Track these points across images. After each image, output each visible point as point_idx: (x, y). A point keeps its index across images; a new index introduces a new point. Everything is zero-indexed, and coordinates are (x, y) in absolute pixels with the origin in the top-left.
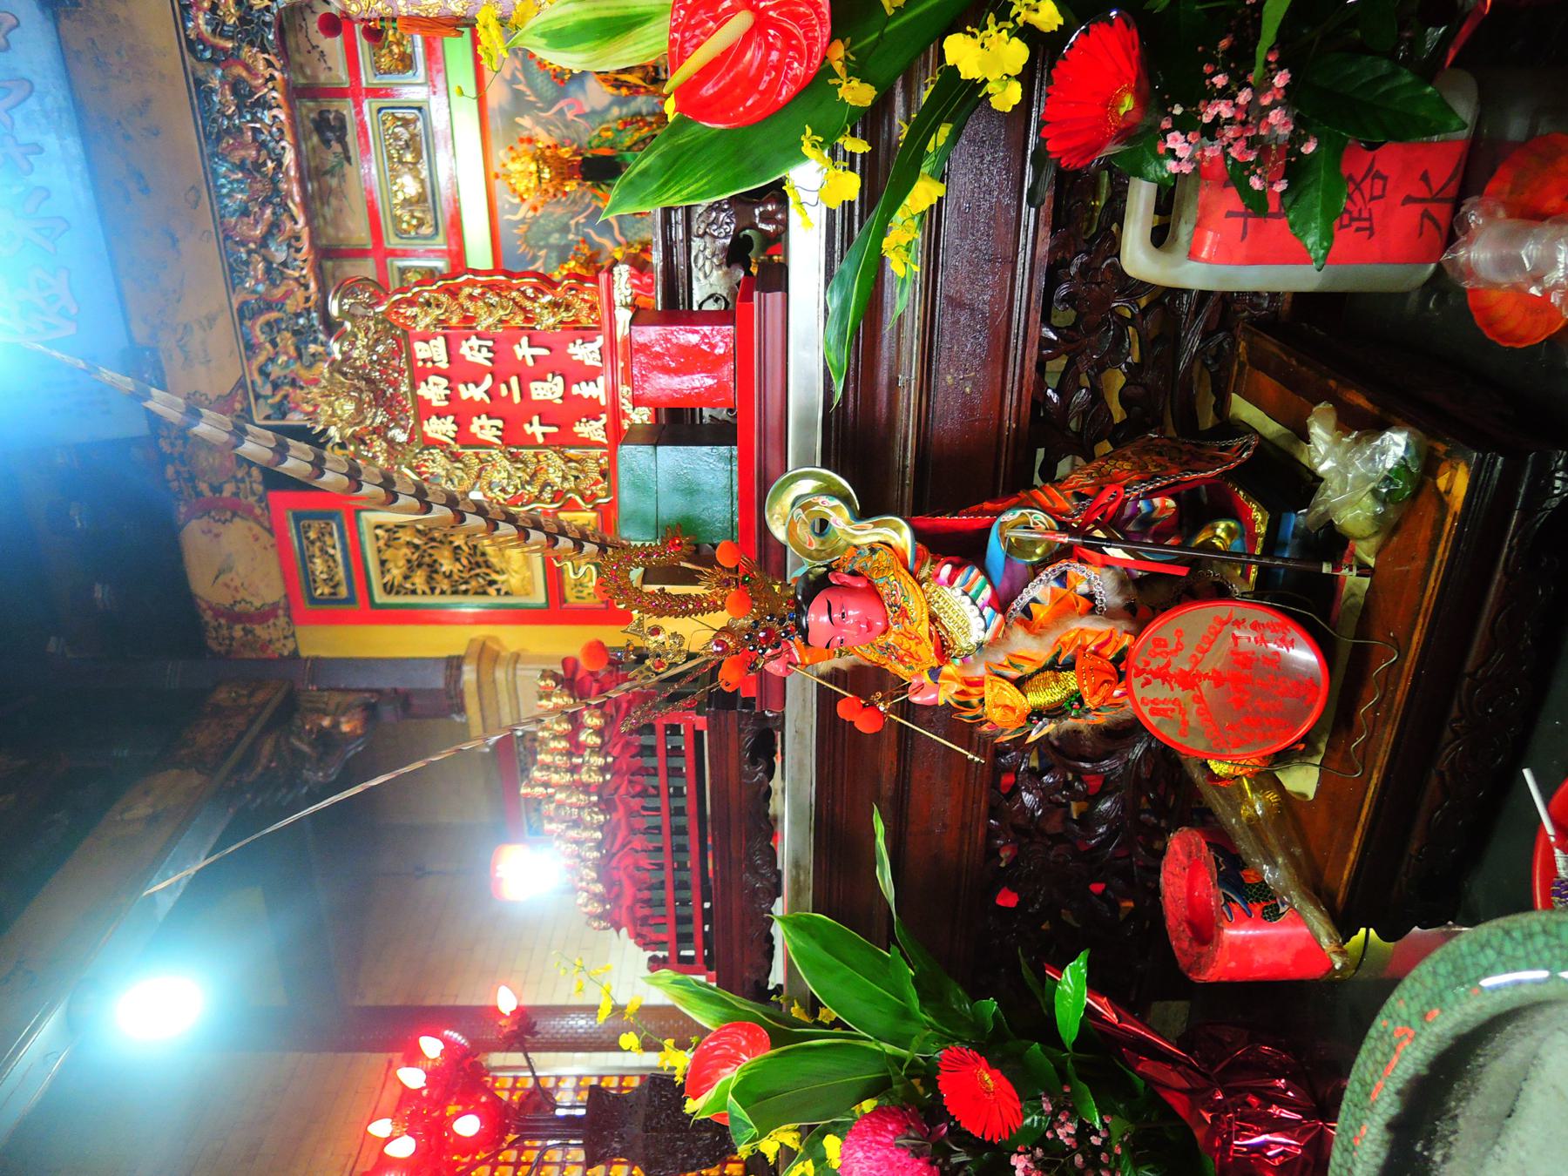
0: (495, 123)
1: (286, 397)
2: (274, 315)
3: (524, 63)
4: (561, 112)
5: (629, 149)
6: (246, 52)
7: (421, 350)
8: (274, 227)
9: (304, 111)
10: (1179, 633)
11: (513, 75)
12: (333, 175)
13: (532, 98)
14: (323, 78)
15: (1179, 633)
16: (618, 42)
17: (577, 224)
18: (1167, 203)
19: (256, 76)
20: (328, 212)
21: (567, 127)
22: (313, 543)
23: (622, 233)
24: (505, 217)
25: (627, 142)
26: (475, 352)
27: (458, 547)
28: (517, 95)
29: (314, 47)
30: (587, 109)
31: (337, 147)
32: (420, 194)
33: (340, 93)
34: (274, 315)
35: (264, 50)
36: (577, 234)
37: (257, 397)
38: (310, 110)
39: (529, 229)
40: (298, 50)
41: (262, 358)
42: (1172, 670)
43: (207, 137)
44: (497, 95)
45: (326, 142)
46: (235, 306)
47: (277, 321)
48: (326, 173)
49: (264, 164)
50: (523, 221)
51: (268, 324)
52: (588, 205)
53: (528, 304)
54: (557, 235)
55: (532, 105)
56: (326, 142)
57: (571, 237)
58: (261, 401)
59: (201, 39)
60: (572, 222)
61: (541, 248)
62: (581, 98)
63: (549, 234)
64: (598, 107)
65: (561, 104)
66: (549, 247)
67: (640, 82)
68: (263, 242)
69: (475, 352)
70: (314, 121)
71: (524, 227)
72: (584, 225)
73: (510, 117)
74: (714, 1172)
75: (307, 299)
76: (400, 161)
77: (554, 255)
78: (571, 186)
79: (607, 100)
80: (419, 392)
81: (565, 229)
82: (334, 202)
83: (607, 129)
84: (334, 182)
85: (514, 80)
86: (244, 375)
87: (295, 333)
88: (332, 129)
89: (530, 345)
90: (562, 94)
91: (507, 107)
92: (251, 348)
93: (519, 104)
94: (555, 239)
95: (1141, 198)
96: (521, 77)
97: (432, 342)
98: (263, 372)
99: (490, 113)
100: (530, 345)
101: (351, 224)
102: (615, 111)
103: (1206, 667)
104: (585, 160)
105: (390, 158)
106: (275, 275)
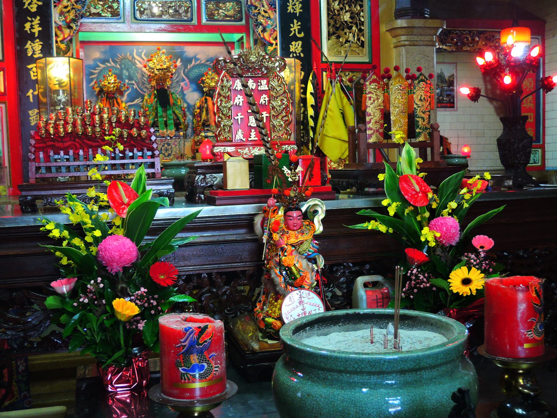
4: (183, 80)
5: (174, 112)
7: (264, 82)
10: (313, 298)
11: (198, 59)
13: (189, 67)
15: (313, 298)
16: (408, 164)
17: (133, 84)
18: (375, 284)
21: (177, 82)
26: (264, 99)
28: (189, 60)
30: (185, 92)
32: (155, 14)
36: (128, 84)
39: (130, 61)
42: (303, 299)
50: (133, 58)
53: (280, 117)
54: (127, 74)
55: (186, 67)
57: (127, 81)
60: (134, 82)
62: (190, 89)
63: (127, 70)
64: (186, 97)
65: (187, 81)
66: (121, 69)
69: (264, 99)
71: (130, 58)
72: (133, 87)
76: (170, 7)
77: (117, 72)
79: (192, 103)
80: (250, 80)
81: (130, 78)
82: (317, 396)
85: (197, 59)
89: (266, 117)
90: (192, 81)
91: (185, 55)
94: (125, 73)
95: (378, 278)
96: (197, 63)
97: (266, 86)
99: (182, 46)
100: (266, 117)
102: (185, 105)
103: (305, 306)
105: (171, 2)
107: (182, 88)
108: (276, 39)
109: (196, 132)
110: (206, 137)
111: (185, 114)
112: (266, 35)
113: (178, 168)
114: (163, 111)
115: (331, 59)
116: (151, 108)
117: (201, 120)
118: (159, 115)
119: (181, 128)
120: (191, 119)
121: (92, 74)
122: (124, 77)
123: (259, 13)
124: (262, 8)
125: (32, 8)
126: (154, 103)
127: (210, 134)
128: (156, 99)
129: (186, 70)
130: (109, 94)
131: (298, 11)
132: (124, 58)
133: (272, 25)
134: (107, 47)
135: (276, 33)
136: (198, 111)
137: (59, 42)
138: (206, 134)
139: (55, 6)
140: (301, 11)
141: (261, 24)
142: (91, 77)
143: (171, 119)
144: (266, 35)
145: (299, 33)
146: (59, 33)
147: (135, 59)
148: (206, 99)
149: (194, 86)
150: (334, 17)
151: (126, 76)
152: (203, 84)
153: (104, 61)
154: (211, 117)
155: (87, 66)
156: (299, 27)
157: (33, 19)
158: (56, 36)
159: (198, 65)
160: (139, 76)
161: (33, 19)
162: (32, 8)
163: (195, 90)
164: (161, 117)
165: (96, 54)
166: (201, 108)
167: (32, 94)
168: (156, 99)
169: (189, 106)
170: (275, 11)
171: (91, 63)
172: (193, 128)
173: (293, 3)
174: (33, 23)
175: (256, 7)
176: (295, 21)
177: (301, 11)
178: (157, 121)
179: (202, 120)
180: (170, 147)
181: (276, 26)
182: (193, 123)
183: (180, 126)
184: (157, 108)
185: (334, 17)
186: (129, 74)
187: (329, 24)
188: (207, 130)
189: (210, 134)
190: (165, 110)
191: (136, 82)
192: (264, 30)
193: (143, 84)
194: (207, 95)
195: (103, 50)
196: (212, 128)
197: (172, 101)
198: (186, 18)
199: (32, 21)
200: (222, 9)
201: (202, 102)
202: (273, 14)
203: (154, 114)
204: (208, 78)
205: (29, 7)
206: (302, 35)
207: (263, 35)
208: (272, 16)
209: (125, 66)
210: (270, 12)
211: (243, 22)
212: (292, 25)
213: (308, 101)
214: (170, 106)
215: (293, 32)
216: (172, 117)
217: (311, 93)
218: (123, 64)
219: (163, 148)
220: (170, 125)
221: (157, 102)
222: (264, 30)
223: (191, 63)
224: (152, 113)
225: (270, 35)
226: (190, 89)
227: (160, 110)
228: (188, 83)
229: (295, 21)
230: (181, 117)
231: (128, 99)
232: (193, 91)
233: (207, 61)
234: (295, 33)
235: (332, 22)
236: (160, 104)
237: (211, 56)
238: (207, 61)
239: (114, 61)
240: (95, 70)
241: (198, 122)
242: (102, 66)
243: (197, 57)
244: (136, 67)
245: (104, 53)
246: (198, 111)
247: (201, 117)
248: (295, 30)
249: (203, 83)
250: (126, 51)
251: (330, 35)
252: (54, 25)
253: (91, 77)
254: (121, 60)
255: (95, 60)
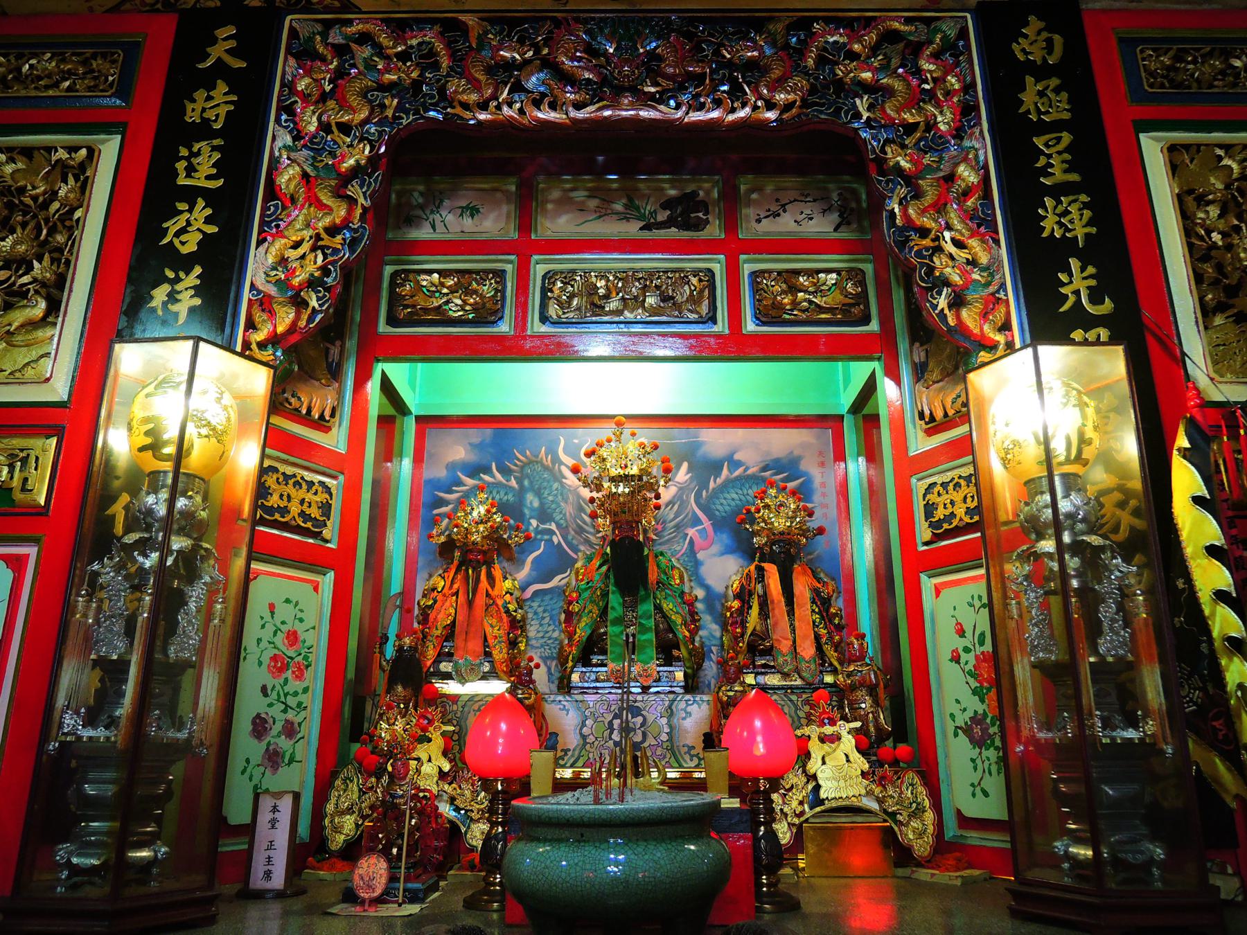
0: (679, 436)
1: (323, 59)
2: (445, 63)
3: (754, 479)
4: (696, 521)
5: (658, 608)
6: (801, 82)
8: (567, 78)
9: (706, 185)
12: (626, 206)
13: (712, 485)
14: (749, 212)
17: (552, 532)
19: (772, 89)
20: (579, 195)
21: (677, 527)
22: (85, 63)
23: (536, 593)
24: (563, 438)
25: (668, 606)
27: (30, 268)
28: (714, 467)
29: (783, 206)
30: (700, 556)
31: (662, 216)
33: (731, 225)
34: (445, 63)
35: (805, 104)
36: (537, 531)
37: (328, 25)
38: (708, 192)
39: (546, 468)
40: (779, 189)
41: (384, 40)
43: (693, 21)
44: (715, 441)
45: (668, 204)
46: (463, 17)
47: (436, 66)
48: (630, 199)
49: (655, 84)
50: (556, 460)
51: (432, 53)
52: (576, 551)
54: (536, 504)
55: (705, 485)
56: (668, 204)
57: (534, 523)
58: (319, 28)
59: (812, 35)
60: (553, 527)
61: (519, 481)
62: (715, 548)
63: (538, 494)
64: (703, 570)
65: (707, 523)
67: (750, 627)
68: (549, 64)
70: (694, 194)
73: (690, 454)
74: (1237, 672)
75: (465, 106)
77: (510, 497)
78: (604, 522)
79: (719, 587)
81: (544, 516)
82: (593, 203)
83: (681, 577)
84: (618, 207)
85: (735, 464)
86: (361, 12)
87: (416, 85)
88: (686, 213)
90: (718, 524)
92: (399, 27)
93: (707, 468)
94: (532, 500)
96: (737, 473)
98: (364, 38)
101: (563, 220)
104: (640, 546)
106: (502, 76)
107: (692, 542)
108: (1005, 327)
109: (730, 675)
110: (764, 689)
111: (693, 613)
112: (969, 316)
113: (581, 840)
114: (624, 605)
115: (1216, 394)
116: (586, 595)
117: (743, 635)
118: (612, 615)
119: (678, 659)
120: (718, 634)
121: (442, 502)
122: (526, 511)
123: (939, 249)
124: (947, 235)
125: (183, 243)
126: (597, 578)
127: (773, 680)
128: (604, 568)
129: (704, 493)
130: (471, 551)
131: (1080, 232)
132: (530, 462)
133: (988, 284)
134: (488, 433)
135: (1003, 309)
136: (736, 604)
137: (254, 346)
138: (761, 679)
139: (260, 243)
140: (1094, 230)
141: (946, 283)
142: (436, 512)
143: (649, 630)
144: (969, 316)
145: (1096, 298)
146: (259, 316)
147: (561, 463)
148: (760, 570)
149: (725, 538)
150: (1213, 253)
151: (532, 509)
152: (751, 524)
153: (475, 470)
154: (775, 624)
155: (429, 482)
156: (1093, 283)
157: (182, 275)
158: (251, 325)
159: (737, 478)
160: (569, 509)
161: (182, 275)
162: (183, 243)
163: (728, 551)
164: (618, 621)
165: (456, 450)
166: (744, 595)
167: (126, 508)
168: (604, 568)
169: (711, 597)
170: (997, 242)
171: (440, 473)
172: (722, 663)
173: (1060, 209)
174: (178, 287)
175: (924, 232)
176: (1074, 264)
177: (1094, 230)
178: (605, 633)
179: (749, 632)
180: (639, 720)
181: (1003, 286)
182: (722, 645)
183: (675, 653)
184: (605, 595)
185: (1213, 253)
186: (542, 504)
187: (1198, 278)
188: (765, 666)
189: (773, 680)
190: (631, 604)
191: (558, 526)
192: (958, 302)
193: (580, 531)
194: (762, 559)
195: (476, 440)
196: (780, 660)
197: (653, 575)
198: (693, 316)
199: (178, 280)
200: (805, 291)
201: (748, 576)
202: (989, 249)
203: (596, 611)
204: (767, 506)
205: (176, 242)
206: (1107, 306)
207: (958, 317)
208: (984, 259)
209: (531, 483)
210: (974, 243)
211: (874, 326)
212: (1063, 277)
213: (1184, 535)
214: (646, 589)
215: (1072, 299)
216: (651, 623)
217: (1197, 500)
218: (528, 476)
219: (616, 722)
220: (644, 647)
221: (606, 576)
222: (958, 302)
223: (718, 475)
224: (589, 607)
225: (984, 315)
226: (715, 548)
227: (615, 600)
228: (710, 530)
229: (1074, 264)
230: (679, 621)
231: (534, 573)
232: (723, 554)
233: (764, 469)
234: (1078, 301)
235: (1209, 269)
236: (617, 584)
237: (775, 456)
238: (764, 469)
239: (505, 471)
240: (450, 492)
241: (736, 639)
242: (470, 482)
243: (736, 457)
244: (562, 483)
245: (479, 447)
246: (736, 604)
247: (743, 624)
248: (1077, 293)
249: (753, 521)
250: (537, 441)
251: (1206, 312)
252: (246, 294)
253: (436, 512)
254: (522, 468)
255: (452, 467)
